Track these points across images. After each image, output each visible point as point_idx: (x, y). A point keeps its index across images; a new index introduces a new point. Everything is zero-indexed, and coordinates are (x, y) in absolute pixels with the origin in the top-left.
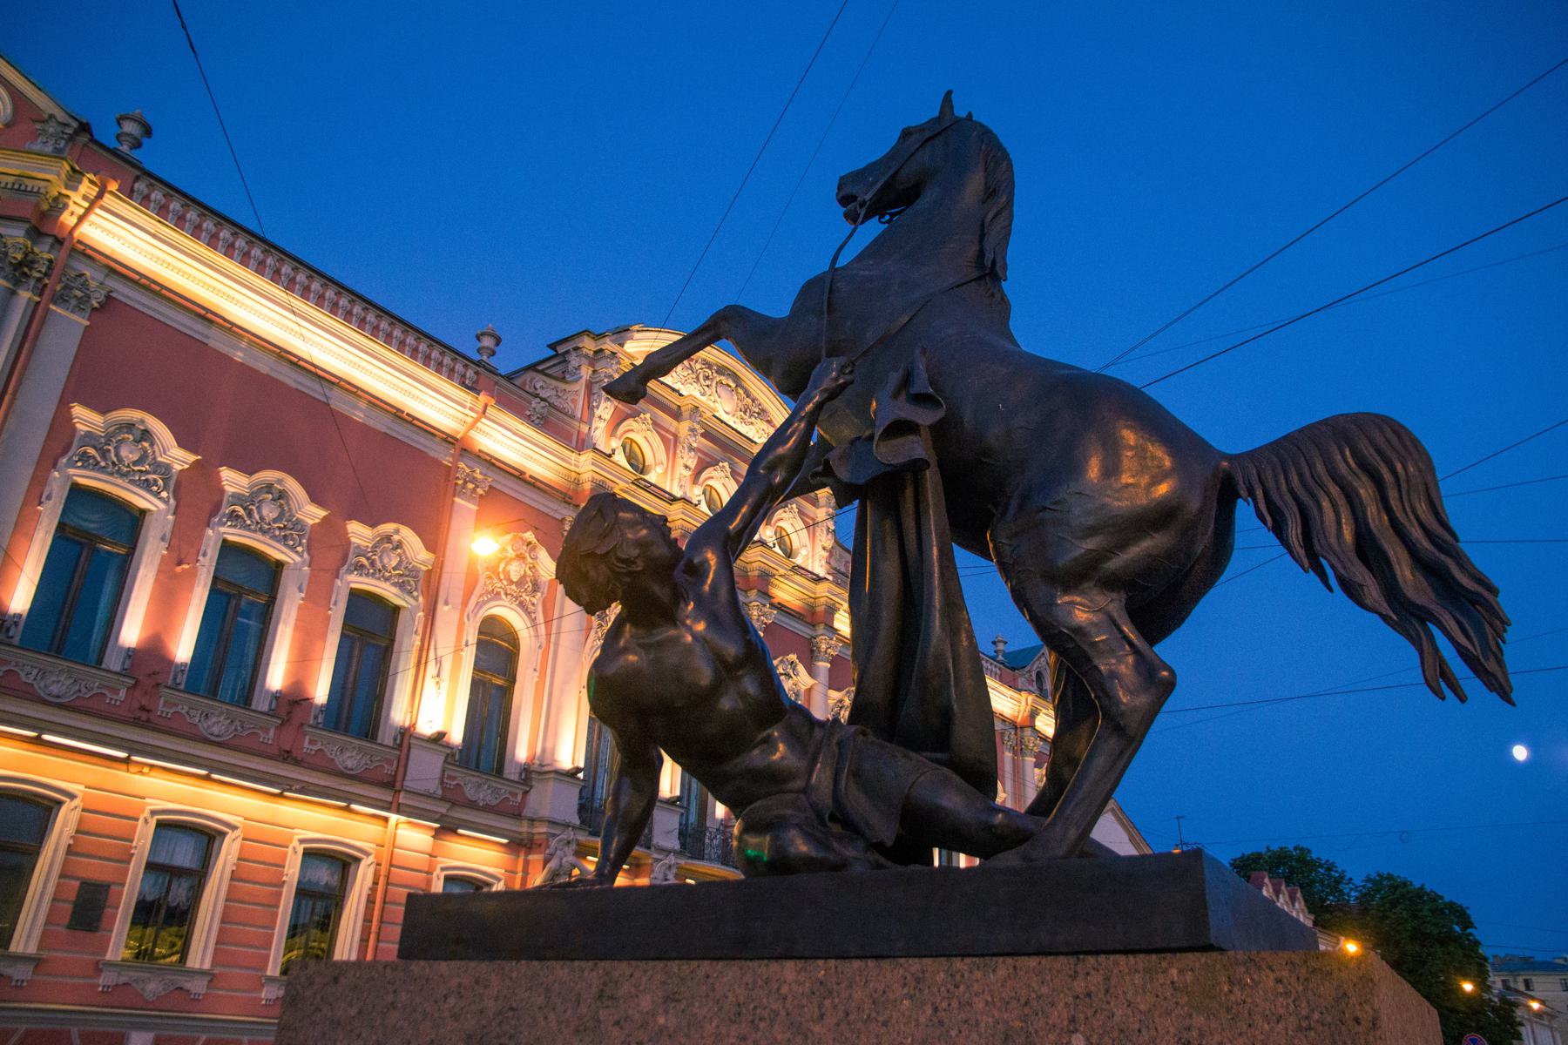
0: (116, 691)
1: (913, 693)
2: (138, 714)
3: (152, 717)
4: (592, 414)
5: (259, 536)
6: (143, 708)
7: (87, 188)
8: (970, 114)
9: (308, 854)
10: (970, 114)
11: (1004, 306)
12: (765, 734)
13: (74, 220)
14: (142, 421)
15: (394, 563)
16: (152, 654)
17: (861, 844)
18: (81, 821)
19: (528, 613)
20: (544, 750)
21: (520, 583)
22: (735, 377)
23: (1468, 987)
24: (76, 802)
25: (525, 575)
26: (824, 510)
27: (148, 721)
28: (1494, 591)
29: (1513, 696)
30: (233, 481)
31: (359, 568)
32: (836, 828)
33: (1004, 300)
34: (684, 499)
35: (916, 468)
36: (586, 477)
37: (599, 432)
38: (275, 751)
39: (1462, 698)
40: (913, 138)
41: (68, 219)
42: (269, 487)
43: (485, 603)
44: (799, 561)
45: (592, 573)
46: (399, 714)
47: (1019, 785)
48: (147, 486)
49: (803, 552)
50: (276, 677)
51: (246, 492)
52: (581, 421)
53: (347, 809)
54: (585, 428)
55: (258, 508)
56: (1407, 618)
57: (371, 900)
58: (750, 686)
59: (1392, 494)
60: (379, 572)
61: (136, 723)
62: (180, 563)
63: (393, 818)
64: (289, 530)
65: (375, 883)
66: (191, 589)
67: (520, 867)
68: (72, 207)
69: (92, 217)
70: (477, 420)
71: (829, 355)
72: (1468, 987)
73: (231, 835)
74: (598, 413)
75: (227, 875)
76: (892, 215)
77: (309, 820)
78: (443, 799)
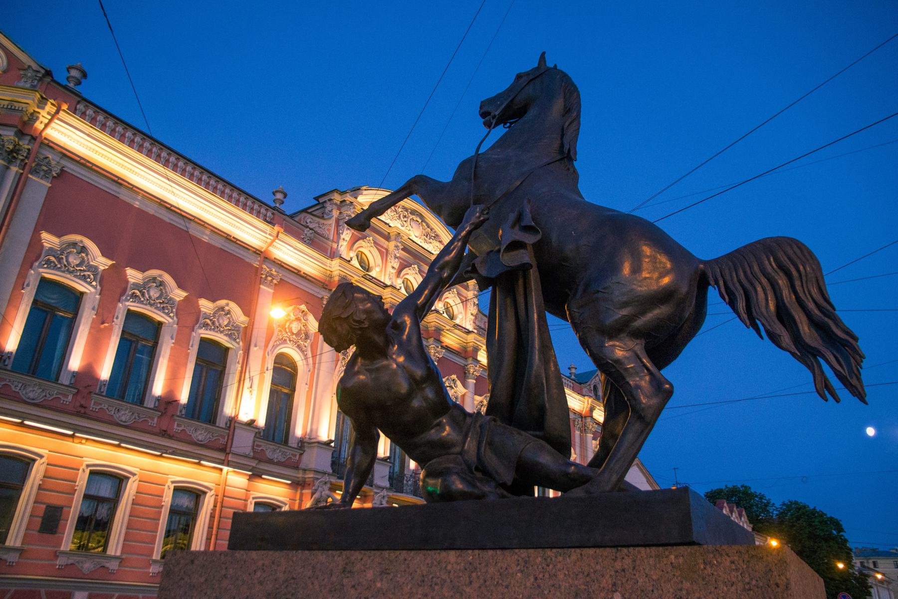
0: (67, 396)
1: (523, 397)
2: (79, 409)
3: (87, 411)
4: (339, 238)
5: (148, 307)
6: (82, 406)
7: (50, 107)
8: (555, 66)
9: (176, 489)
10: (555, 66)
11: (575, 175)
12: (438, 421)
13: (42, 126)
14: (82, 242)
15: (226, 323)
16: (87, 375)
17: (493, 484)
18: (46, 470)
19: (303, 351)
20: (311, 430)
21: (298, 334)
22: (421, 216)
24: (43, 460)
25: (301, 330)
26: (472, 292)
27: (85, 413)
28: (855, 339)
29: (866, 399)
30: (133, 276)
31: (206, 325)
32: (479, 475)
33: (575, 172)
34: (392, 286)
35: (524, 268)
36: (336, 273)
37: (343, 248)
38: (157, 430)
39: (837, 400)
40: (523, 79)
41: (39, 126)
42: (154, 279)
43: (277, 346)
44: (457, 321)
45: (339, 328)
46: (228, 409)
48: (84, 278)
49: (460, 316)
50: (158, 388)
51: (141, 282)
52: (333, 241)
53: (199, 464)
54: (335, 246)
55: (148, 291)
57: (212, 516)
58: (430, 393)
59: (797, 283)
60: (217, 328)
61: (78, 414)
62: (103, 323)
63: (225, 469)
64: (165, 304)
65: (215, 506)
66: (109, 338)
67: (298, 497)
68: (41, 119)
69: (53, 125)
70: (273, 241)
71: (475, 203)
72: (841, 566)
73: (132, 479)
74: (342, 237)
75: (130, 501)
76: (511, 123)
77: (177, 470)
78: (254, 458)
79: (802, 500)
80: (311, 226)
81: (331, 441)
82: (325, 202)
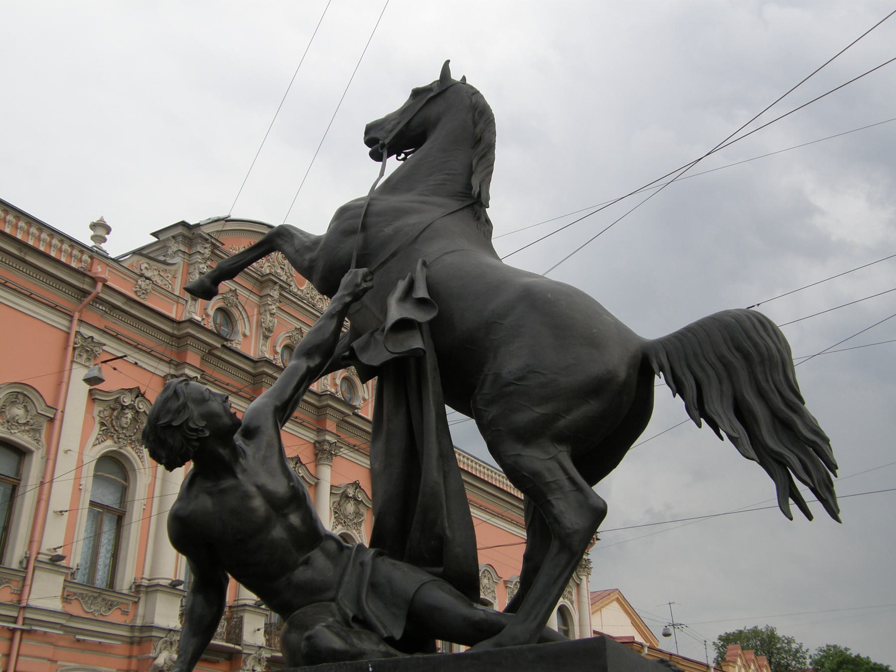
8: (464, 78)
10: (464, 78)
11: (486, 226)
12: (305, 557)
17: (374, 638)
23: (100, 270)
28: (826, 440)
29: (840, 516)
32: (356, 627)
33: (488, 221)
35: (417, 356)
39: (809, 517)
45: (170, 441)
47: (498, 597)
56: (773, 463)
58: (295, 519)
59: (759, 370)
71: (358, 266)
72: (100, 270)
76: (407, 154)
79: (842, 645)
80: (148, 274)
81: (180, 583)
82: (168, 239)
